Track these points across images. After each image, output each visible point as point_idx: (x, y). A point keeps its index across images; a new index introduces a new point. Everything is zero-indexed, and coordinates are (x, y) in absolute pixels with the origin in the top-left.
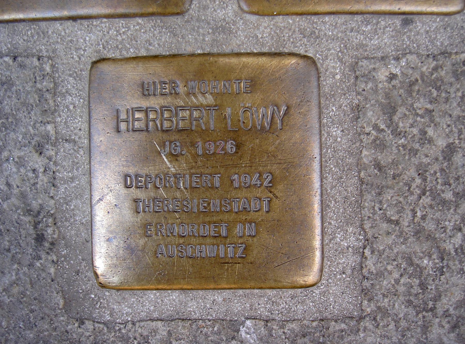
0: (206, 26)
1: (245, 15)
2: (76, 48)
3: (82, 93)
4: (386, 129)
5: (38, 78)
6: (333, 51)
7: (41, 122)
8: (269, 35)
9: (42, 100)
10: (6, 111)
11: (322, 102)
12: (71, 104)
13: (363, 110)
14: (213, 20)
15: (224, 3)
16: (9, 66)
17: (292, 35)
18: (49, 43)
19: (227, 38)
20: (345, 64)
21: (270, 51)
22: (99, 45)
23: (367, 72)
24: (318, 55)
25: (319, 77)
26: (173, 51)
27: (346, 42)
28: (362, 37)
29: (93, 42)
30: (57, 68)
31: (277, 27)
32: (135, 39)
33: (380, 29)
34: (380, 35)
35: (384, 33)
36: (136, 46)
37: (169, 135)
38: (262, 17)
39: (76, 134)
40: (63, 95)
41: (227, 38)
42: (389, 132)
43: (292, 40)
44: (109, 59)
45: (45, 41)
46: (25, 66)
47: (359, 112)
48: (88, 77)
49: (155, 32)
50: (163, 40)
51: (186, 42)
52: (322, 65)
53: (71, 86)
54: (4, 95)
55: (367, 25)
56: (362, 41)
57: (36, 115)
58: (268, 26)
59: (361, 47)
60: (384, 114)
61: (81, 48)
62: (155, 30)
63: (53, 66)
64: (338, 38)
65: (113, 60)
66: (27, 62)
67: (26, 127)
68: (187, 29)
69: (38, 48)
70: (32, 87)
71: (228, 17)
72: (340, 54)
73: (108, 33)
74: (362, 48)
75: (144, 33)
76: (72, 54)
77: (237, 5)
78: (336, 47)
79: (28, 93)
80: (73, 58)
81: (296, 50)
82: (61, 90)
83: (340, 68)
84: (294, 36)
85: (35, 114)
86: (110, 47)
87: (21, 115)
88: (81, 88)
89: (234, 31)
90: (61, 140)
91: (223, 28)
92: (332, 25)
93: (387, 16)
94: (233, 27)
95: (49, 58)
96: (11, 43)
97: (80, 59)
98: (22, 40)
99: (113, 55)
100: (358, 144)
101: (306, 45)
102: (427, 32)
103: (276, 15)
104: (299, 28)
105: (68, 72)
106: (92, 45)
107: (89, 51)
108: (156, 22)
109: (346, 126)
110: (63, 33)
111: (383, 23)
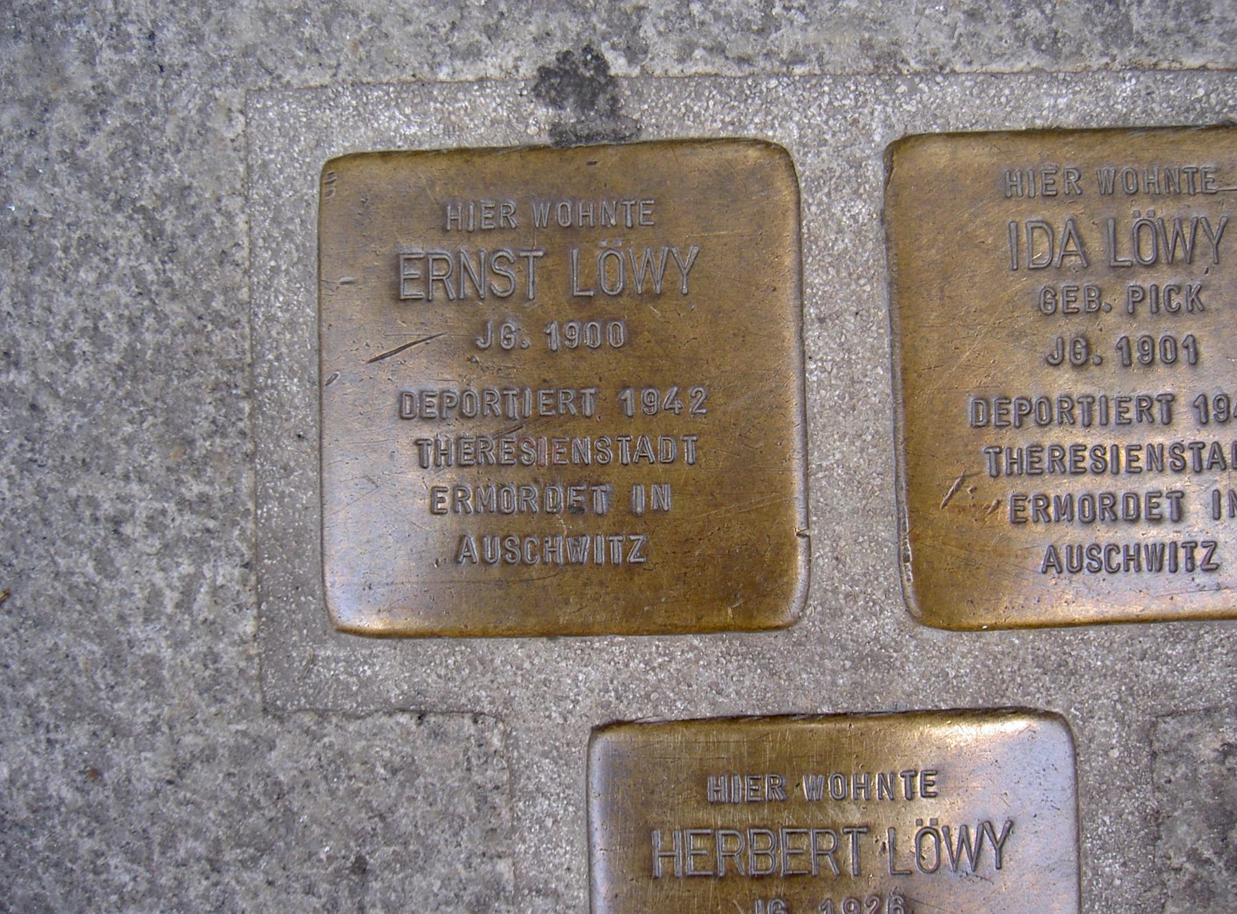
2: (555, 697)
3: (571, 792)
4: (1215, 859)
5: (474, 761)
7: (484, 854)
8: (973, 669)
9: (485, 808)
10: (403, 829)
11: (1082, 806)
12: (548, 815)
13: (1167, 821)
15: (875, 603)
16: (409, 734)
18: (495, 685)
19: (882, 679)
21: (973, 706)
22: (607, 691)
23: (1175, 743)
25: (791, 166)
27: (1131, 680)
28: (1164, 669)
29: (593, 684)
30: (516, 738)
33: (1202, 650)
35: (1210, 659)
36: (688, 696)
37: (765, 887)
39: (558, 879)
40: (531, 798)
42: (1221, 864)
43: (1019, 680)
44: (631, 722)
45: (486, 680)
46: (445, 734)
47: (1158, 826)
48: (585, 759)
49: (730, 666)
50: (747, 683)
52: (1081, 729)
53: (546, 777)
54: (399, 795)
57: (470, 838)
58: (970, 652)
59: (1162, 690)
60: (1211, 827)
61: (568, 697)
62: (730, 662)
63: (506, 735)
64: (1114, 674)
65: (641, 724)
66: (451, 725)
67: (450, 865)
69: (471, 695)
70: (461, 780)
72: (1119, 707)
73: (627, 665)
75: (704, 666)
76: (547, 709)
77: (903, 608)
79: (453, 793)
80: (549, 717)
81: (1027, 701)
82: (525, 786)
83: (1120, 736)
84: (1023, 672)
85: (471, 838)
87: (437, 838)
88: (568, 781)
89: (898, 664)
90: (526, 892)
91: (876, 658)
92: (1103, 646)
93: (1216, 623)
95: (498, 717)
96: (408, 681)
97: (565, 719)
98: (434, 676)
99: (640, 715)
100: (1156, 891)
101: (1048, 690)
104: (1033, 654)
105: (540, 748)
106: (592, 691)
107: (585, 703)
108: (731, 643)
109: (1131, 855)
110: (527, 665)
111: (1208, 638)
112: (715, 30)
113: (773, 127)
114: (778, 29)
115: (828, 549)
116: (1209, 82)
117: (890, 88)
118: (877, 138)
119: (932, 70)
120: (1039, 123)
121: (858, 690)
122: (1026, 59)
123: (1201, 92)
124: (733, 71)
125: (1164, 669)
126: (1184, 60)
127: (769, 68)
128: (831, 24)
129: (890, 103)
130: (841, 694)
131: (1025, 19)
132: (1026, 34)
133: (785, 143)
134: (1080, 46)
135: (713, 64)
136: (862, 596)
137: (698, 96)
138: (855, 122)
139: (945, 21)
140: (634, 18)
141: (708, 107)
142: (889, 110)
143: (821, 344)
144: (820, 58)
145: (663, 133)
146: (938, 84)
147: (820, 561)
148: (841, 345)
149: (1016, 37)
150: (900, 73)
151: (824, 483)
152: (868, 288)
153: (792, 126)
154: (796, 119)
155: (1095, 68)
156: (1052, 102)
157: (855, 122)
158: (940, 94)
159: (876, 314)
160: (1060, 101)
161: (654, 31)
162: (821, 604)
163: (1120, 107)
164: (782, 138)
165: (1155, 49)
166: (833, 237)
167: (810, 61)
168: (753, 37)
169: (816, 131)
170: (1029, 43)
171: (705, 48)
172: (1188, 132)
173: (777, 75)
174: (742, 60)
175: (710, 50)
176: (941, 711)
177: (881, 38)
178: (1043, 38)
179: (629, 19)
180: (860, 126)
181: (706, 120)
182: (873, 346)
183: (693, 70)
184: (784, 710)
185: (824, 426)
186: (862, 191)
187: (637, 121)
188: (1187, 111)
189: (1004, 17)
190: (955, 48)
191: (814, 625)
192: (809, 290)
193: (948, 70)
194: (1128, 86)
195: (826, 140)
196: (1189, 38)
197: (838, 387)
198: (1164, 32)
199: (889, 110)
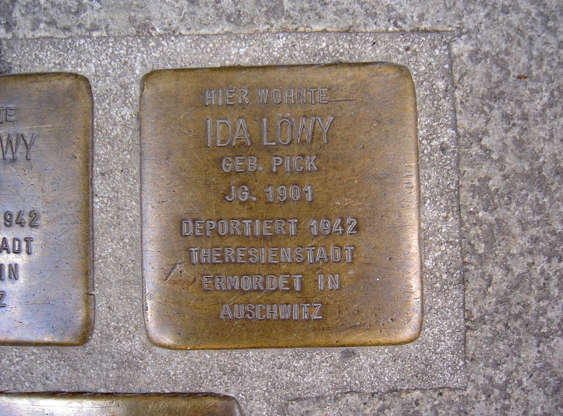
0: (110, 360)
1: (155, 348)
6: (258, 390)
14: (118, 353)
15: (130, 333)
17: (210, 372)
19: (134, 375)
20: (273, 405)
21: (184, 391)
24: (240, 395)
25: (89, 88)
26: (73, 388)
27: (274, 379)
28: (293, 374)
31: (192, 363)
32: (30, 371)
33: (315, 364)
34: (314, 371)
36: (31, 380)
38: (174, 351)
41: (134, 375)
43: (210, 377)
49: (53, 364)
50: (62, 374)
51: (87, 378)
52: (246, 406)
55: (298, 360)
56: (293, 378)
58: (182, 361)
62: (52, 362)
68: (89, 362)
71: (135, 349)
72: (267, 394)
74: (294, 387)
75: (40, 364)
78: (262, 385)
81: (215, 390)
83: (268, 410)
84: (212, 373)
86: (3, 379)
93: (323, 349)
94: (141, 361)
99: (7, 389)
102: (372, 366)
103: (190, 349)
104: (217, 364)
111: (318, 357)
112: (52, 12)
113: (81, 66)
114: (85, 11)
115: (104, 302)
116: (329, 39)
117: (145, 43)
118: (138, 72)
119: (169, 34)
120: (228, 63)
121: (121, 380)
122: (221, 26)
123: (324, 45)
124: (61, 35)
125: (293, 374)
126: (313, 26)
127: (80, 33)
128: (114, 8)
129: (145, 53)
130: (111, 382)
131: (222, 4)
132: (223, 12)
133: (87, 75)
134: (252, 19)
135: (49, 31)
136: (123, 328)
137: (42, 49)
138: (126, 63)
139: (176, 5)
140: (11, 7)
141: (47, 55)
142: (145, 56)
143: (102, 188)
144: (107, 27)
145: (22, 70)
146: (172, 41)
147: (100, 309)
148: (113, 188)
149: (217, 14)
150: (151, 35)
151: (102, 265)
152: (128, 157)
153: (92, 65)
154: (94, 61)
155: (262, 31)
156: (237, 51)
157: (126, 63)
158: (173, 47)
159: (132, 171)
160: (241, 50)
161: (19, 13)
162: (101, 332)
163: (276, 53)
164: (85, 72)
165: (296, 20)
166: (111, 128)
167: (102, 29)
168: (72, 16)
169: (104, 68)
170: (224, 18)
171: (46, 22)
172: (313, 68)
173: (84, 37)
174: (66, 29)
175: (49, 24)
176: (165, 393)
177: (140, 15)
178: (232, 14)
179: (8, 7)
180: (129, 65)
181: (46, 62)
182: (130, 189)
183: (39, 35)
184: (81, 390)
185: (103, 234)
186: (127, 102)
187: (10, 63)
188: (315, 55)
189: (211, 3)
190: (182, 20)
191: (97, 344)
192: (96, 158)
193: (177, 33)
194: (281, 42)
195: (109, 73)
196: (316, 14)
197: (111, 212)
198: (302, 10)
199: (145, 56)
